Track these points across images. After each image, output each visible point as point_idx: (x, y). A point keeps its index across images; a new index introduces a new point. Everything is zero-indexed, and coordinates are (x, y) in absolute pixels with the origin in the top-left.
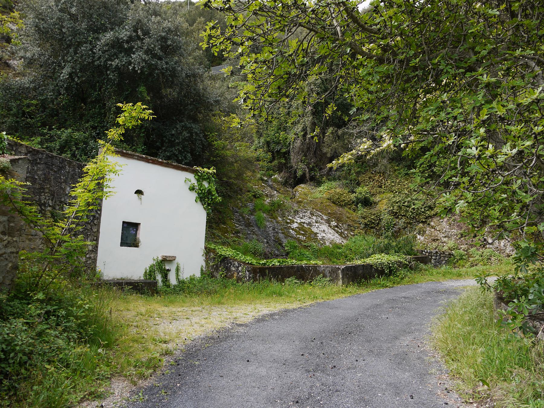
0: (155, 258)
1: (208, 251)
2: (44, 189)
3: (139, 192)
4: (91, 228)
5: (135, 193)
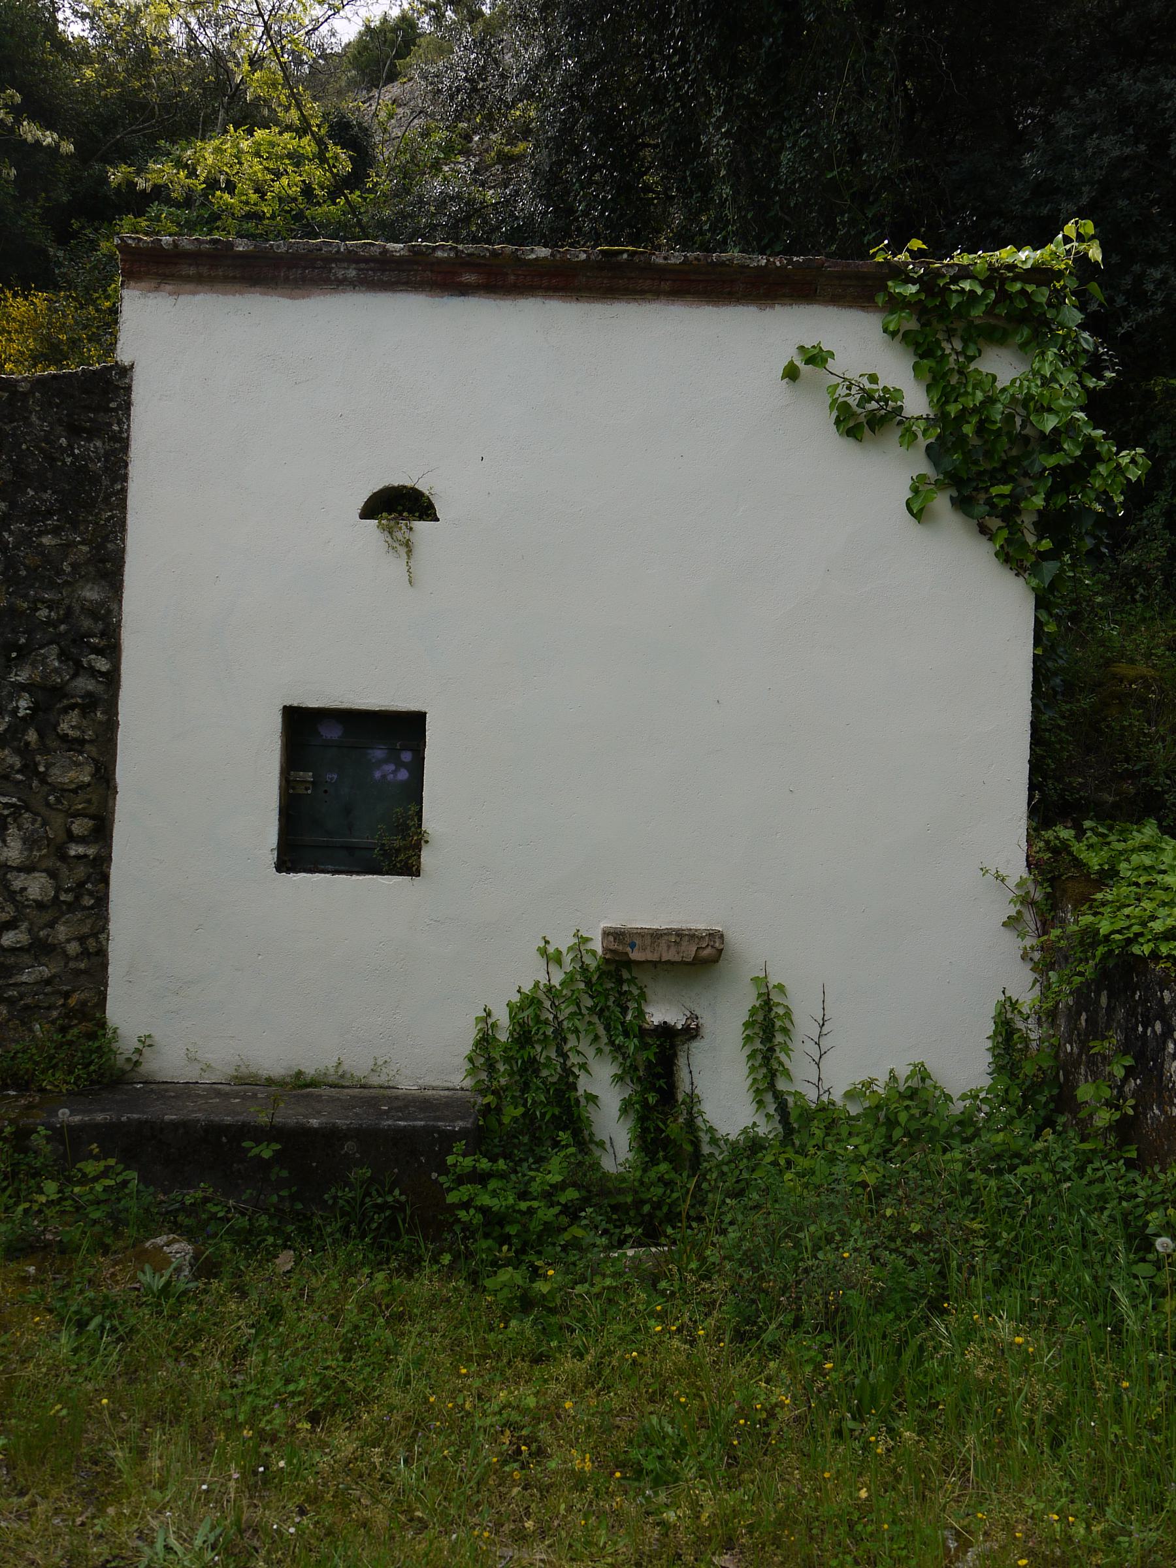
0: (563, 942)
1: (1056, 883)
3: (399, 506)
4: (29, 768)
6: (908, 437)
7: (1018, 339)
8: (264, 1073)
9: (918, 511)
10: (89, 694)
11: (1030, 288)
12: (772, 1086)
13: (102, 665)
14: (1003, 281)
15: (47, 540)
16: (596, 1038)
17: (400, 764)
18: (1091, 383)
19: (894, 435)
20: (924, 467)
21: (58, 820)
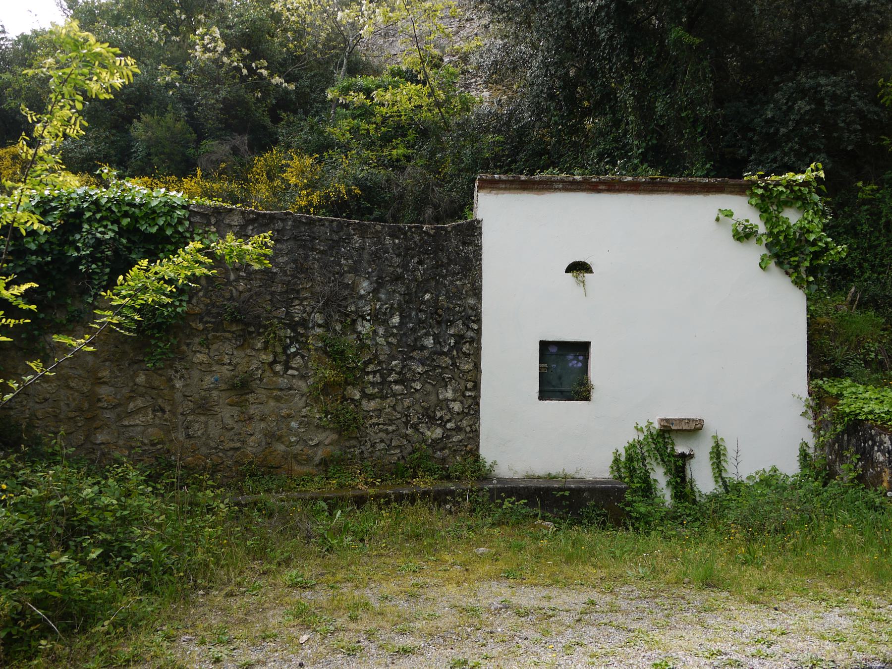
0: (643, 424)
1: (819, 401)
2: (298, 292)
3: (579, 268)
5: (566, 272)
6: (759, 240)
7: (798, 205)
8: (537, 474)
9: (763, 267)
10: (472, 337)
11: (802, 189)
12: (720, 475)
13: (475, 327)
14: (792, 186)
15: (458, 283)
16: (657, 459)
17: (578, 361)
18: (824, 221)
19: (753, 240)
20: (765, 251)
21: (463, 383)
